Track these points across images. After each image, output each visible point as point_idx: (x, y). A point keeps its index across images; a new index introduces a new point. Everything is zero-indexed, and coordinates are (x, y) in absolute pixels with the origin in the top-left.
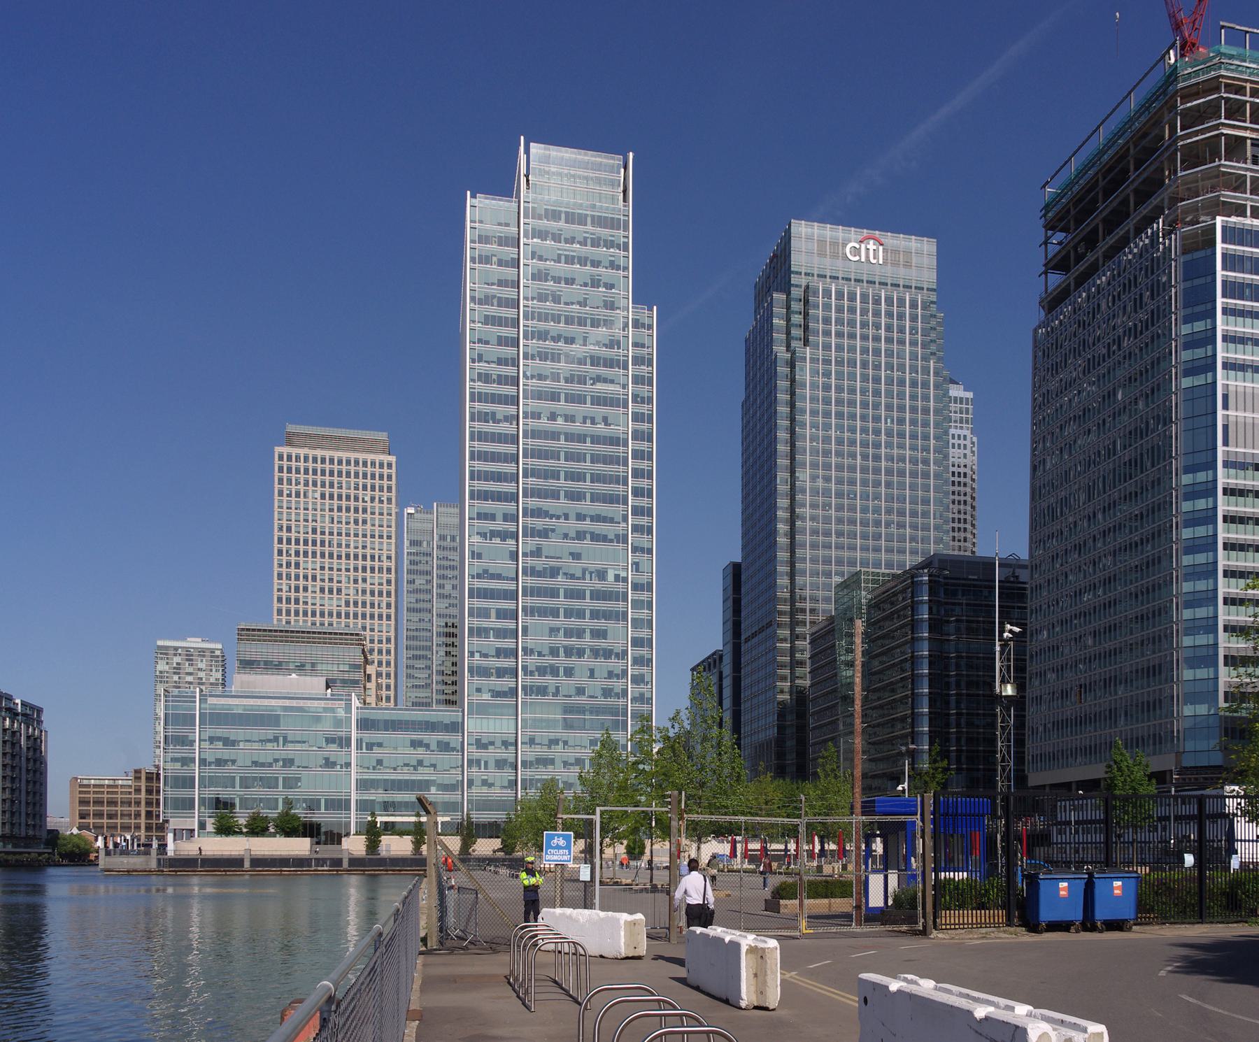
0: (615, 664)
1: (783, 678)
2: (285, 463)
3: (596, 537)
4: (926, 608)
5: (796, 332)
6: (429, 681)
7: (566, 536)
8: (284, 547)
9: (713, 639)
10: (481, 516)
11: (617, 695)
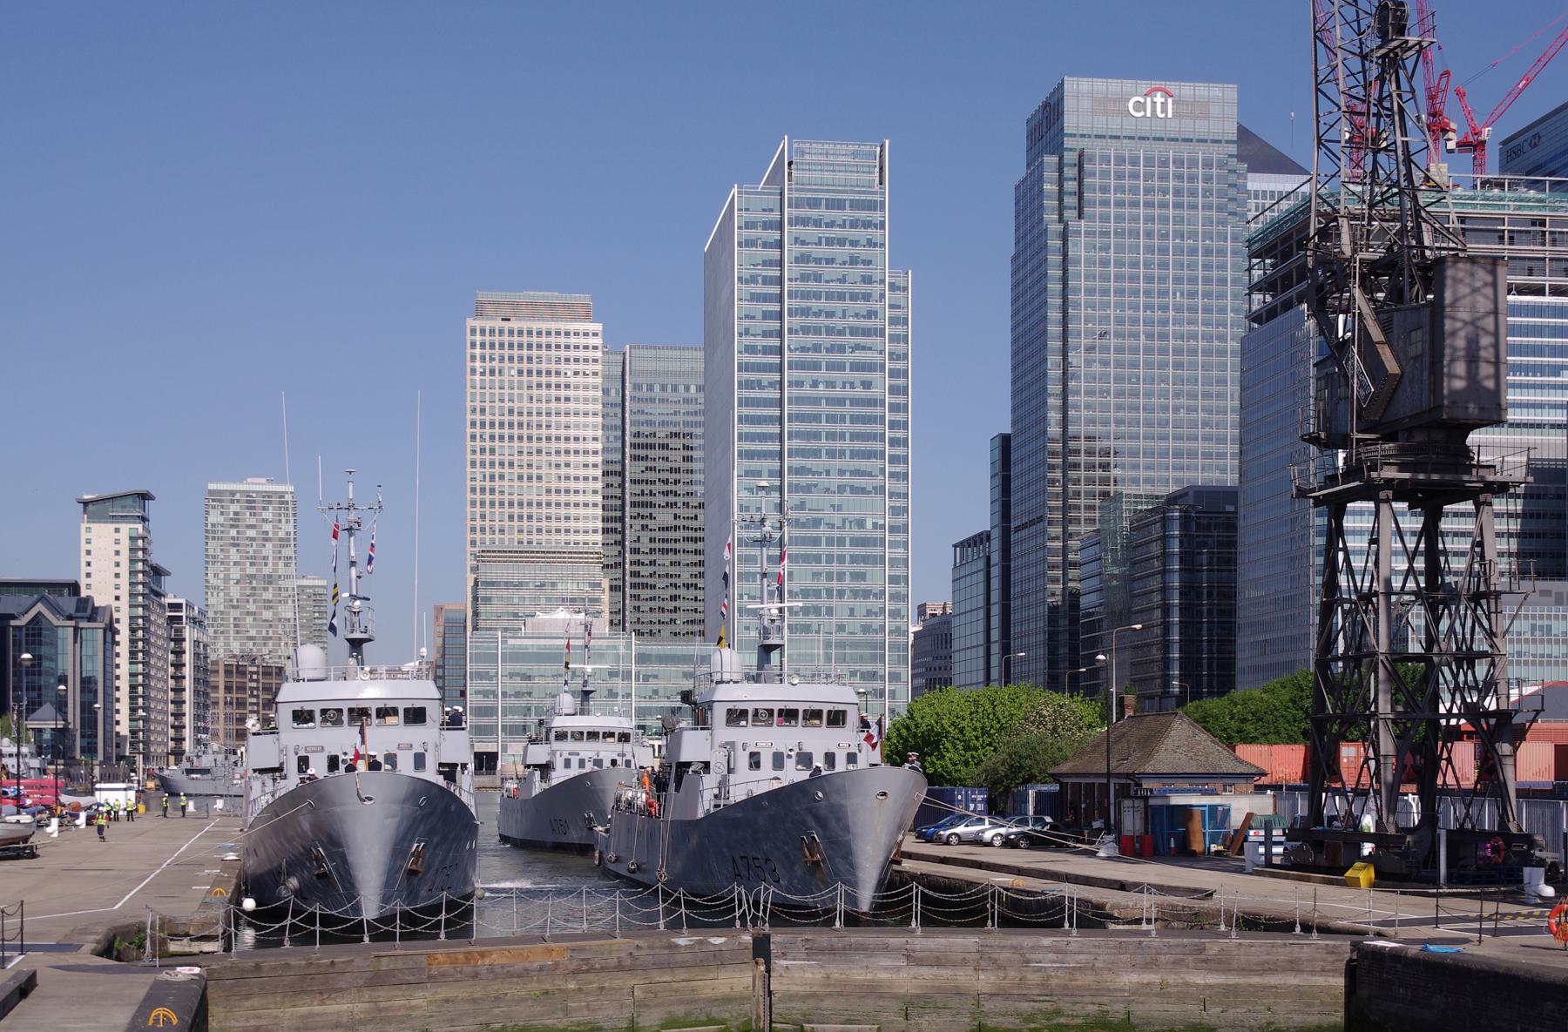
0: (873, 603)
1: (1055, 580)
2: (478, 338)
3: (855, 490)
4: (1176, 542)
5: (1070, 201)
6: (619, 560)
7: (827, 490)
8: (478, 431)
9: (979, 517)
10: (749, 473)
11: (876, 631)
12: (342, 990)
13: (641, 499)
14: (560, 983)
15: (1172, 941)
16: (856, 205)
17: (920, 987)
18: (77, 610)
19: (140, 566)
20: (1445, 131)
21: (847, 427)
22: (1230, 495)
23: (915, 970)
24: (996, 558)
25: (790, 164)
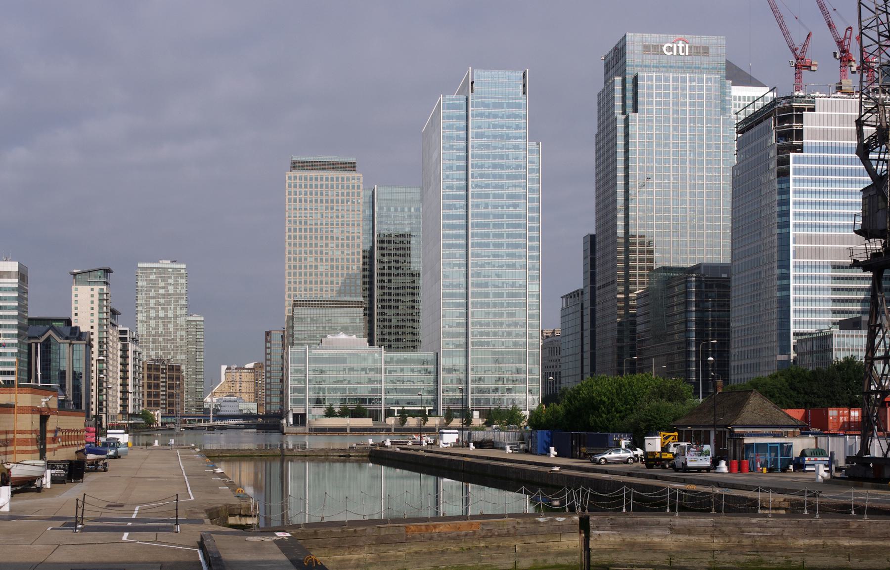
3: (509, 266)
9: (577, 281)
12: (360, 546)
13: (383, 271)
14: (476, 543)
15: (829, 520)
16: (509, 106)
17: (679, 546)
18: (71, 334)
19: (105, 309)
20: (850, 61)
21: (505, 231)
22: (724, 268)
23: (675, 537)
24: (587, 304)
25: (472, 83)
